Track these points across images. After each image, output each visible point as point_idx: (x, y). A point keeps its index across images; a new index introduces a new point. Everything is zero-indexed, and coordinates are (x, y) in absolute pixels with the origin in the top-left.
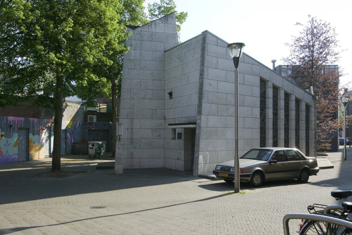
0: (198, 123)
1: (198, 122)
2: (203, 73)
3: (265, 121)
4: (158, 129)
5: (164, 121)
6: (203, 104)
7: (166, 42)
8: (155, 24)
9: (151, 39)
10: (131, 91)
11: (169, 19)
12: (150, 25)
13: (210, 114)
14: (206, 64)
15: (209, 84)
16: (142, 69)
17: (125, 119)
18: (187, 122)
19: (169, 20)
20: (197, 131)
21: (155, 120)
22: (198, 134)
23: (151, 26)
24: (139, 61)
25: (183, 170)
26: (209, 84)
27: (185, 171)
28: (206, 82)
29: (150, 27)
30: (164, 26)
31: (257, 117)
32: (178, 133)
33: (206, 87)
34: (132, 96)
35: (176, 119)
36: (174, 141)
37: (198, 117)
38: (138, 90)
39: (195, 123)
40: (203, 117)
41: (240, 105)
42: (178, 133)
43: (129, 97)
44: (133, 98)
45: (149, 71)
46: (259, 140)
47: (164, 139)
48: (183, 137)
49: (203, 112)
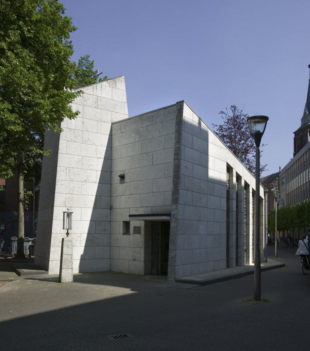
0: (174, 214)
1: (173, 213)
2: (180, 152)
3: (229, 214)
4: (103, 221)
5: (110, 211)
6: (181, 191)
7: (114, 111)
8: (101, 87)
9: (96, 104)
10: (70, 170)
11: (118, 82)
12: (95, 87)
13: (186, 203)
14: (183, 142)
15: (186, 167)
16: (84, 142)
17: (61, 208)
18: (150, 213)
19: (117, 84)
20: (172, 224)
21: (100, 209)
22: (173, 229)
23: (96, 89)
24: (81, 132)
25: (143, 273)
26: (186, 167)
27: (145, 275)
28: (183, 163)
29: (95, 89)
30: (111, 91)
31: (224, 209)
32: (134, 227)
33: (183, 171)
34: (72, 177)
35: (131, 209)
36: (126, 237)
37: (174, 207)
38: (79, 169)
39: (169, 215)
40: (179, 206)
41: (211, 194)
42: (134, 227)
43: (68, 178)
44: (72, 180)
45: (92, 146)
46: (226, 236)
47: (110, 235)
48: (142, 232)
49: (181, 200)
